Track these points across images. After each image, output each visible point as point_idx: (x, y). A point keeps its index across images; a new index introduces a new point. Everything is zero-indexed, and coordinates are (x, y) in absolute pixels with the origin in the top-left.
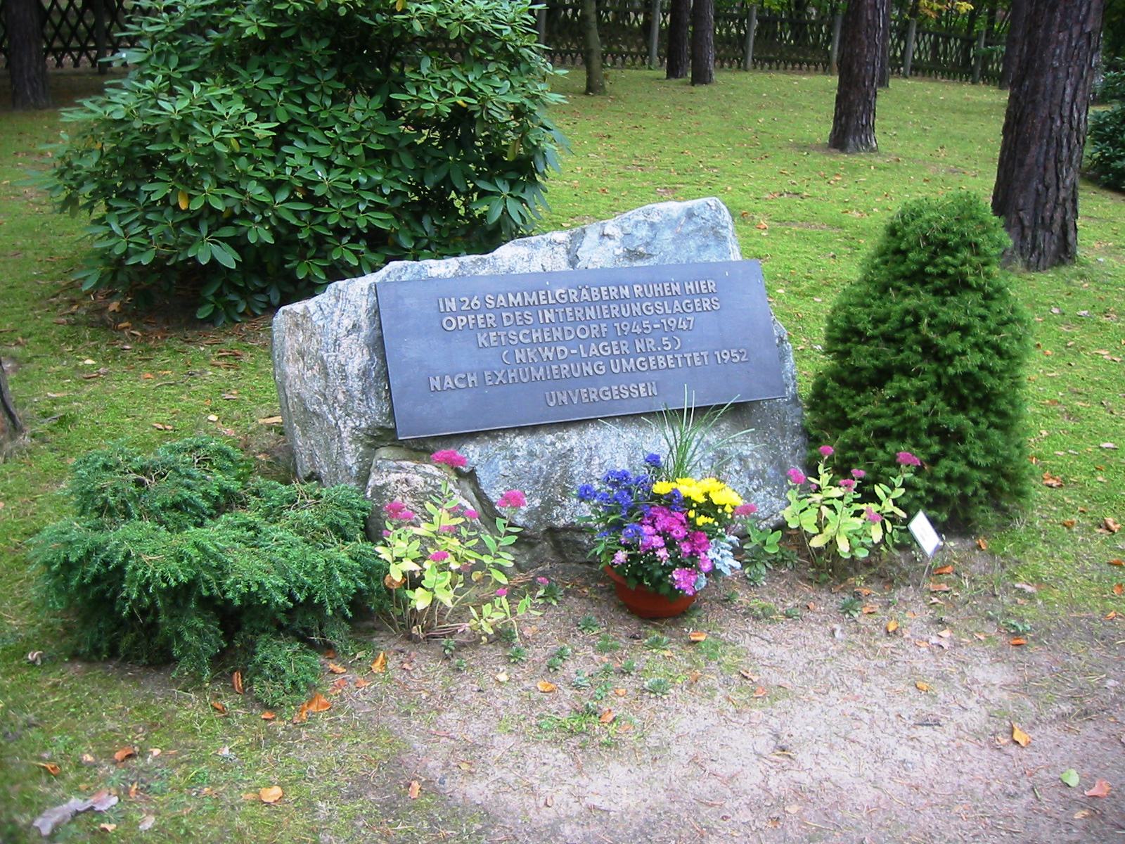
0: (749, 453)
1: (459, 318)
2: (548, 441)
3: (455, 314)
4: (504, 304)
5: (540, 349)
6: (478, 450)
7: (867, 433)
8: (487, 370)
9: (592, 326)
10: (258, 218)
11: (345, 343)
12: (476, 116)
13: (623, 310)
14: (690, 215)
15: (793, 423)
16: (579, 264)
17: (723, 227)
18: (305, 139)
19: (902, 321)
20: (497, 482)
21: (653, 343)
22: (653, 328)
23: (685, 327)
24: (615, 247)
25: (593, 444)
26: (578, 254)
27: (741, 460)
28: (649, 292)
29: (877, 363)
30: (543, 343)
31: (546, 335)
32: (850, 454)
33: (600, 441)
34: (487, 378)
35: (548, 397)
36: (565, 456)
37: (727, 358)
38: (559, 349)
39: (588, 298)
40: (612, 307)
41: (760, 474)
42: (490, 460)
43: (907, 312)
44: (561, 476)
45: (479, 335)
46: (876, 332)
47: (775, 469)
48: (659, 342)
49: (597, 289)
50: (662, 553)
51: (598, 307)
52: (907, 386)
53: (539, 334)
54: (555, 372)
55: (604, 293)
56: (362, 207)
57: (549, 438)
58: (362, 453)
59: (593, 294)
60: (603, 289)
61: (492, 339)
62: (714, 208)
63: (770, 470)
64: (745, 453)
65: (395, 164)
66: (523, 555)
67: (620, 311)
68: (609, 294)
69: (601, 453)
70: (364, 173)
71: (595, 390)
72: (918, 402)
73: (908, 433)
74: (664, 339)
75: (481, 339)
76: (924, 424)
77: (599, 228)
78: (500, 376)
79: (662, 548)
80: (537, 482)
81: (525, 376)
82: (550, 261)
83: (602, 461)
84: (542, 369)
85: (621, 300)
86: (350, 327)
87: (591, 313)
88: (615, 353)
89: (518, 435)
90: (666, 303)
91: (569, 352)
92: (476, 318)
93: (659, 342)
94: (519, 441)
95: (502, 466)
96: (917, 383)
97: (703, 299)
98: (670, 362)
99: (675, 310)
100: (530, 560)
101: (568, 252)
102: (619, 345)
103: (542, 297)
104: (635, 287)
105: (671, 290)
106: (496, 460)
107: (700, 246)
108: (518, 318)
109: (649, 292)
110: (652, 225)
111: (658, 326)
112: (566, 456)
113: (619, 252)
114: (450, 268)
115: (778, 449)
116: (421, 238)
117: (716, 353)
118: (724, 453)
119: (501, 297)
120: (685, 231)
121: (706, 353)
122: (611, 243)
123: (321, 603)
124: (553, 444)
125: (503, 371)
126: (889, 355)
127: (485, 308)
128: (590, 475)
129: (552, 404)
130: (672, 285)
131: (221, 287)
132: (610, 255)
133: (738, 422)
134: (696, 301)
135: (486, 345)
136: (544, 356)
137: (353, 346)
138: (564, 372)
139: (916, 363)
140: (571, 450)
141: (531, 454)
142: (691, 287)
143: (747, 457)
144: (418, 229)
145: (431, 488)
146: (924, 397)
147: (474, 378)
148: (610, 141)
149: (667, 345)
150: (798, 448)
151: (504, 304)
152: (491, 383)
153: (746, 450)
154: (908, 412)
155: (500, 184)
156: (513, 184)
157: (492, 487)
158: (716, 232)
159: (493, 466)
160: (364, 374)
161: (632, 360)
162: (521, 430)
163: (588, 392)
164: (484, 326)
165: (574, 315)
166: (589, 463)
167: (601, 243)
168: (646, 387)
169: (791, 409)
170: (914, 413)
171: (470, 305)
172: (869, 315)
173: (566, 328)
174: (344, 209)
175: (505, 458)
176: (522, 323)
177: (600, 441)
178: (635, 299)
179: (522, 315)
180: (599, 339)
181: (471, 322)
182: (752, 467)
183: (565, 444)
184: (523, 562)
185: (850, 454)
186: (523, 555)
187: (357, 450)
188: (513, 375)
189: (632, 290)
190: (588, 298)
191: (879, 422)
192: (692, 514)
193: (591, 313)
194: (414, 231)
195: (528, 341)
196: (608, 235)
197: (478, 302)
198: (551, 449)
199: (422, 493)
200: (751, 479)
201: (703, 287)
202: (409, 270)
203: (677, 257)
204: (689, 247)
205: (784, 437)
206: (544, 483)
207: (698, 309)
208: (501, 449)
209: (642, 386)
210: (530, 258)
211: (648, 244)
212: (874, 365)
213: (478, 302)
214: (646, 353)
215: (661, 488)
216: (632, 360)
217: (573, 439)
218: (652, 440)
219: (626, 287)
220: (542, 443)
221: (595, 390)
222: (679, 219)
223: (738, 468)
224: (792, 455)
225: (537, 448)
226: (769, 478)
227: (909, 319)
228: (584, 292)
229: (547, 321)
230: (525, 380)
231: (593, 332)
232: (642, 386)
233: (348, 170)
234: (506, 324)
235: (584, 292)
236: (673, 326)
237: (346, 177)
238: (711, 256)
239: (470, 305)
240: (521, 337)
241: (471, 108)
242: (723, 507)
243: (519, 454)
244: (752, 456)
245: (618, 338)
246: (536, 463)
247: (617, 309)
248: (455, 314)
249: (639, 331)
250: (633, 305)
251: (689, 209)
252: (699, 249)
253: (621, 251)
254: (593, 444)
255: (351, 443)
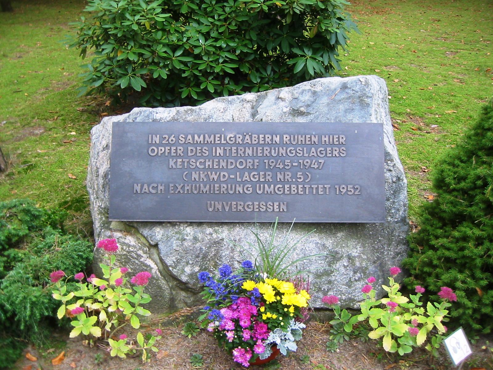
0: (357, 254)
1: (160, 148)
2: (208, 232)
3: (157, 145)
4: (191, 141)
5: (209, 173)
6: (162, 232)
7: (439, 259)
8: (171, 183)
9: (249, 160)
10: (161, 65)
11: (101, 154)
12: (286, 11)
13: (273, 151)
14: (344, 87)
15: (399, 236)
16: (258, 116)
17: (367, 97)
18: (199, 22)
19: (474, 183)
20: (171, 253)
21: (290, 176)
22: (292, 165)
23: (316, 166)
24: (284, 106)
25: (238, 238)
26: (258, 109)
27: (349, 258)
28: (294, 140)
29: (454, 210)
30: (212, 169)
31: (215, 164)
32: (426, 269)
33: (243, 236)
34: (171, 188)
35: (209, 205)
36: (218, 243)
37: (344, 191)
38: (222, 174)
39: (249, 141)
40: (265, 148)
41: (363, 270)
42: (168, 238)
43: (479, 178)
44: (215, 255)
45: (171, 160)
46: (458, 186)
47: (376, 267)
48: (294, 176)
49: (256, 136)
50: (230, 335)
51: (255, 148)
52: (469, 232)
53: (210, 163)
54: (216, 189)
55: (261, 139)
56: (221, 61)
57: (209, 230)
58: (104, 221)
59: (253, 139)
60: (261, 136)
61: (179, 163)
62: (363, 83)
63: (371, 268)
64: (353, 254)
65: (247, 37)
66: (189, 297)
67: (270, 152)
68: (265, 140)
69: (242, 244)
70: (225, 42)
71: (242, 203)
72: (477, 246)
73: (467, 265)
74: (299, 173)
75: (172, 163)
76: (479, 262)
77: (276, 93)
78: (179, 187)
79: (232, 330)
80: (198, 257)
81: (196, 190)
82: (238, 113)
83: (242, 250)
84: (208, 186)
85: (272, 144)
86: (105, 146)
87: (249, 151)
88: (262, 180)
89: (189, 226)
90: (305, 149)
91: (229, 176)
92: (170, 150)
93: (294, 176)
94: (189, 230)
95: (175, 244)
96: (477, 232)
97: (334, 148)
98: (300, 189)
99: (312, 154)
100: (193, 301)
101: (253, 108)
102: (265, 175)
103: (217, 139)
104: (285, 136)
105: (311, 140)
106: (172, 240)
107: (347, 110)
108: (198, 151)
109: (294, 140)
110: (314, 93)
111: (296, 164)
112: (218, 243)
113: (285, 110)
114: (171, 114)
115: (383, 253)
116: (265, 78)
117: (337, 187)
118: (337, 253)
119: (190, 137)
120: (337, 98)
121: (329, 186)
122: (282, 104)
123: (19, 321)
124: (211, 234)
125: (182, 185)
126: (463, 206)
127: (177, 144)
128: (232, 258)
129: (210, 210)
130: (313, 137)
131: (149, 99)
132: (279, 111)
133: (353, 232)
134: (328, 149)
135: (174, 167)
136: (211, 177)
137: (104, 158)
138: (222, 189)
139: (479, 216)
140: (222, 240)
141: (195, 239)
142: (327, 139)
143: (355, 257)
144: (264, 73)
145: (125, 253)
146: (481, 244)
147: (162, 188)
148: (439, 23)
149: (300, 178)
150: (400, 253)
151: (191, 141)
152: (172, 192)
153: (355, 253)
154: (466, 252)
155: (306, 51)
156: (315, 51)
157: (167, 256)
158: (362, 100)
159: (169, 243)
160: (105, 176)
161: (272, 186)
162: (191, 224)
163: (237, 205)
164: (175, 154)
165: (237, 152)
166: (233, 250)
167: (275, 103)
168: (279, 205)
169: (400, 227)
170: (470, 254)
171: (168, 140)
172: (455, 173)
173: (230, 161)
174: (211, 62)
175: (178, 239)
176: (200, 155)
177: (243, 236)
178: (282, 144)
179: (201, 150)
180: (250, 170)
181: (167, 151)
182: (358, 264)
183: (219, 235)
184: (189, 302)
185: (426, 269)
186: (189, 297)
187: (101, 219)
188: (188, 188)
189: (282, 138)
190: (249, 141)
191: (447, 253)
192: (262, 309)
193: (249, 151)
194: (261, 73)
195: (202, 167)
196: (281, 98)
197: (174, 139)
198: (209, 237)
199: (119, 255)
200: (355, 273)
201: (335, 140)
202: (143, 114)
203: (328, 116)
204: (339, 109)
205: (389, 245)
206: (203, 258)
207: (328, 155)
208: (176, 233)
209: (276, 204)
210: (225, 110)
211: (308, 106)
212: (452, 211)
213: (174, 139)
214: (283, 182)
215: (248, 285)
216: (272, 186)
217: (224, 233)
218: (281, 239)
219: (278, 136)
220: (203, 233)
221: (242, 203)
222: (335, 89)
223: (346, 264)
224: (393, 258)
225: (200, 236)
226: (369, 273)
227: (479, 183)
228: (247, 137)
229: (218, 155)
230: (195, 192)
231: (248, 164)
232: (276, 204)
233: (216, 40)
234: (190, 154)
235: (247, 137)
236: (308, 165)
237: (214, 44)
238: (355, 118)
239: (168, 140)
240: (198, 164)
241: (284, 7)
242: (288, 307)
243: (188, 238)
244: (359, 257)
245: (265, 170)
246: (198, 245)
247: (269, 150)
248: (157, 145)
249: (281, 166)
250: (281, 149)
251: (345, 83)
252: (346, 111)
253: (288, 109)
254: (238, 238)
255: (98, 214)
